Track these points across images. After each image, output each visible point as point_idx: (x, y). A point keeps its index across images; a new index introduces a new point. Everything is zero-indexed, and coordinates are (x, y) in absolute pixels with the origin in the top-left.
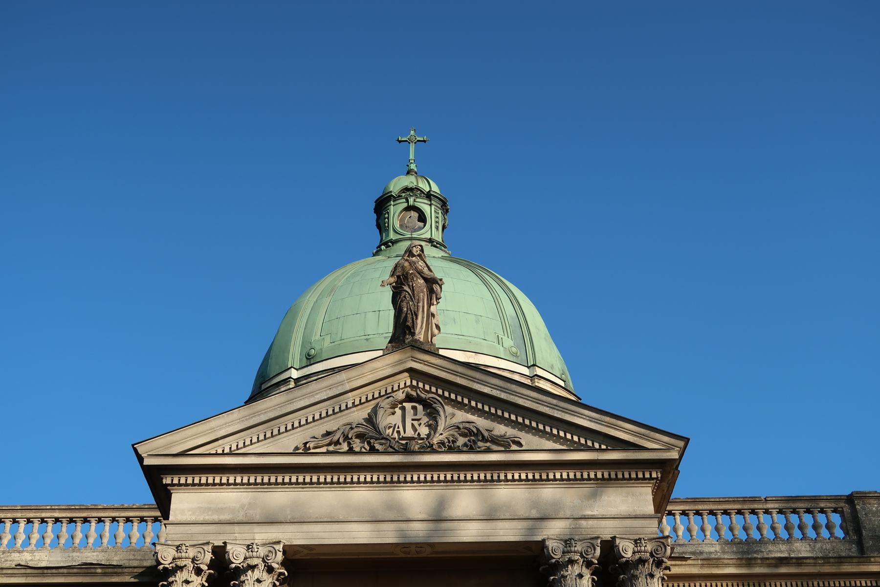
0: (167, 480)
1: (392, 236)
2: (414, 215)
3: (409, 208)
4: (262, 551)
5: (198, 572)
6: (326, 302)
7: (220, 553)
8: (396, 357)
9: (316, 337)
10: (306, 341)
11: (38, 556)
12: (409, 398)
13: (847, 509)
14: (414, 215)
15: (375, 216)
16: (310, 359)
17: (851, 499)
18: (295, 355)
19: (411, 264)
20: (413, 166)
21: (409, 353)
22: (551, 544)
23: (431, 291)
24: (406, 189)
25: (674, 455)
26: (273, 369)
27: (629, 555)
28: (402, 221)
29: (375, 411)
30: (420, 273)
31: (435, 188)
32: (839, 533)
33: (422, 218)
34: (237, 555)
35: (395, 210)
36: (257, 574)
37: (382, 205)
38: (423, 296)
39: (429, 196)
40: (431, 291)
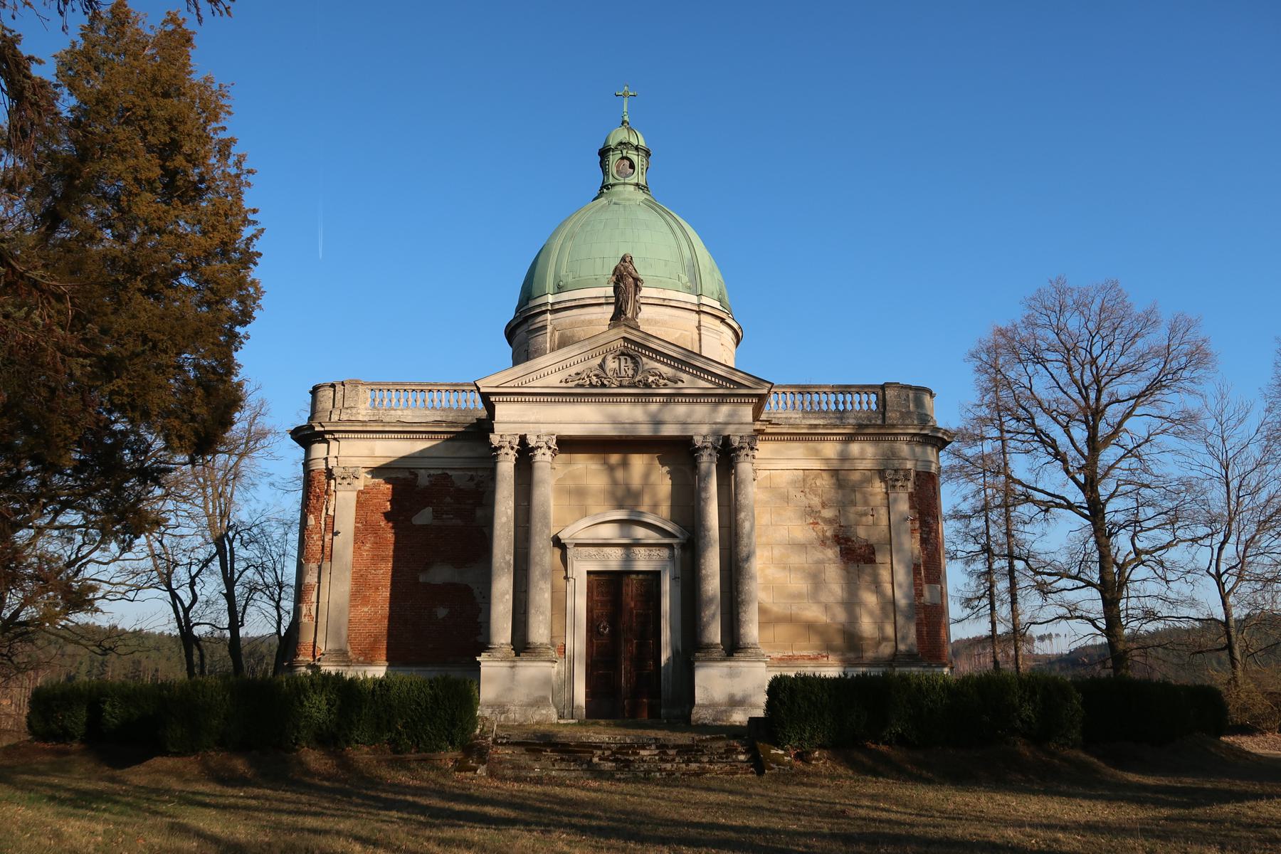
0: (492, 399)
1: (611, 181)
2: (627, 163)
3: (623, 158)
4: (545, 439)
5: (512, 448)
6: (569, 244)
7: (523, 439)
8: (615, 331)
9: (563, 273)
10: (556, 275)
11: (406, 412)
12: (623, 354)
13: (880, 393)
14: (627, 163)
15: (599, 158)
16: (560, 289)
17: (883, 387)
18: (550, 285)
19: (625, 268)
20: (626, 118)
21: (623, 328)
22: (696, 438)
23: (636, 286)
24: (621, 143)
25: (765, 391)
26: (536, 292)
27: (736, 444)
28: (618, 167)
29: (604, 360)
30: (630, 274)
31: (642, 143)
32: (874, 407)
33: (632, 166)
34: (532, 442)
35: (613, 158)
36: (543, 450)
37: (604, 153)
38: (632, 290)
39: (637, 148)
40: (636, 286)
